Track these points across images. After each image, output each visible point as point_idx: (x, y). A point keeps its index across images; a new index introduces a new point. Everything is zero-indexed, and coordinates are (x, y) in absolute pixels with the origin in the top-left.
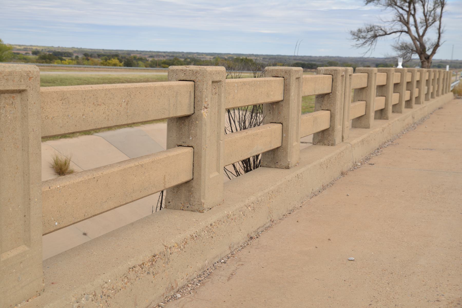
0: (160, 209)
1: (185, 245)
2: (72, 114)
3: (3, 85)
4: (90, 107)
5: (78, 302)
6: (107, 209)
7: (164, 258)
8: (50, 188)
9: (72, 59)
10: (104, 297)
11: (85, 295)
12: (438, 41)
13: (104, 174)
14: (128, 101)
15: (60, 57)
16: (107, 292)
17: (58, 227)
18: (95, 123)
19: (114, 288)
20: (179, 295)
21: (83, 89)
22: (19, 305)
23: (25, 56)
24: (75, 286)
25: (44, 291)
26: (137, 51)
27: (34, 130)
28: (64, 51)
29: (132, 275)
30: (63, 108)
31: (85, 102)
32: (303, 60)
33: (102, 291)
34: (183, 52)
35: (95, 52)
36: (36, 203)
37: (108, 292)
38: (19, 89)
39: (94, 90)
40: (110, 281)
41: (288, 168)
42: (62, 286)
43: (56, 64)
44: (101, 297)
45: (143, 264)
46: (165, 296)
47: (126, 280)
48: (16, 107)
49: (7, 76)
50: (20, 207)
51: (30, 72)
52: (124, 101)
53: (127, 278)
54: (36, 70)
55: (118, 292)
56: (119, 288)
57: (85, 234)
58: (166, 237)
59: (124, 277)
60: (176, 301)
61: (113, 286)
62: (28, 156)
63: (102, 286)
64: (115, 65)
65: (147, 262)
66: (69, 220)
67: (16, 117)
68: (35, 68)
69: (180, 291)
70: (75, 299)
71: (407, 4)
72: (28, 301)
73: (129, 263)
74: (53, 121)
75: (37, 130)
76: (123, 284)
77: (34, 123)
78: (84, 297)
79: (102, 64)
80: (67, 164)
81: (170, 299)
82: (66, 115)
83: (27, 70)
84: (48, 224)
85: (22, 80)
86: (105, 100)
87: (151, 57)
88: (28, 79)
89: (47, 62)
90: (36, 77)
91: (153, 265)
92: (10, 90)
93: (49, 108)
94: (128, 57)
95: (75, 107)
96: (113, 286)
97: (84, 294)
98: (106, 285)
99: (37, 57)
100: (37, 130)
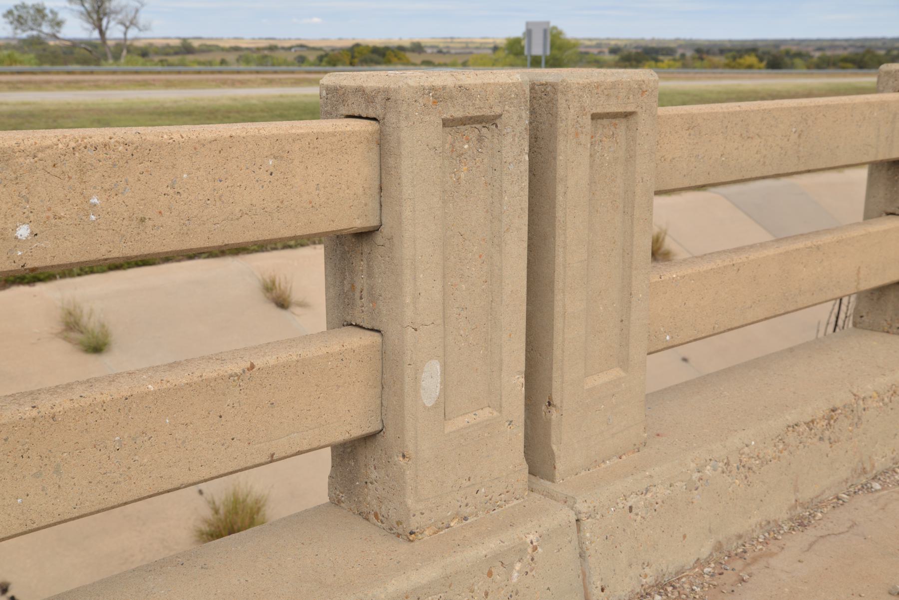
0: (834, 330)
1: (893, 398)
2: (703, 153)
3: (602, 105)
4: (734, 142)
5: (699, 472)
6: (752, 320)
7: (851, 416)
8: (661, 278)
9: (674, 60)
10: (742, 469)
11: (712, 462)
13: (750, 259)
14: (802, 131)
16: (748, 461)
17: (670, 345)
18: (742, 169)
19: (761, 456)
20: (877, 486)
21: (725, 110)
22: (608, 462)
24: (695, 445)
25: (645, 446)
27: (644, 180)
28: (661, 45)
29: (791, 438)
30: (690, 144)
31: (726, 132)
33: (740, 459)
36: (640, 302)
37: (750, 462)
38: (625, 111)
39: (744, 111)
40: (753, 443)
42: (674, 442)
44: (738, 469)
45: (813, 421)
46: (849, 484)
47: (781, 446)
48: (618, 141)
49: (609, 90)
50: (615, 305)
51: (644, 81)
52: (794, 130)
53: (784, 442)
54: (653, 78)
55: (767, 463)
56: (769, 458)
57: (685, 360)
58: (857, 379)
59: (777, 440)
60: (870, 494)
61: (759, 453)
62: (632, 222)
63: (740, 450)
64: (750, 67)
65: (820, 420)
66: (689, 334)
67: (618, 158)
68: (652, 75)
69: (879, 479)
70: (695, 465)
72: (620, 458)
73: (787, 417)
74: (672, 165)
75: (648, 179)
76: (775, 452)
77: (644, 167)
78: (710, 465)
79: (728, 66)
80: (660, 240)
81: (859, 490)
82: (695, 155)
83: (639, 79)
84: (654, 337)
85: (631, 96)
86: (761, 129)
87: (819, 49)
88: (640, 93)
90: (652, 91)
91: (830, 425)
92: (610, 113)
93: (667, 144)
94: (774, 51)
95: (710, 141)
96: (759, 453)
97: (710, 460)
98: (746, 450)
99: (616, 57)
100: (648, 179)
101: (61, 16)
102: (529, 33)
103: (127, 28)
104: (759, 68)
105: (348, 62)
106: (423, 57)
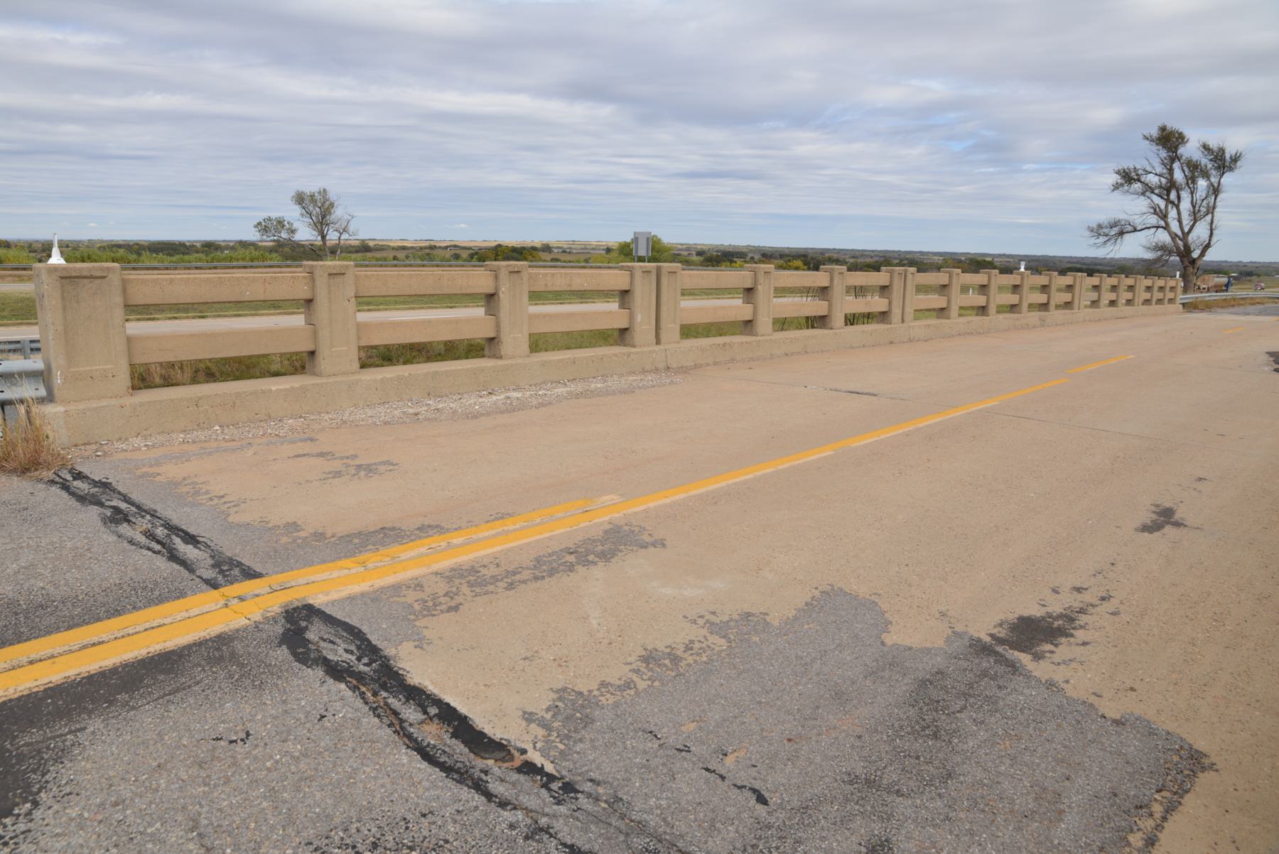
12: (1210, 240)
15: (730, 258)
23: (687, 258)
26: (834, 249)
28: (737, 250)
32: (1081, 264)
34: (899, 251)
35: (777, 251)
41: (832, 329)
43: (723, 268)
64: (797, 268)
71: (1165, 192)
89: (713, 266)
99: (701, 258)
101: (296, 225)
102: (636, 240)
103: (341, 234)
104: (804, 270)
105: (493, 258)
106: (552, 256)
